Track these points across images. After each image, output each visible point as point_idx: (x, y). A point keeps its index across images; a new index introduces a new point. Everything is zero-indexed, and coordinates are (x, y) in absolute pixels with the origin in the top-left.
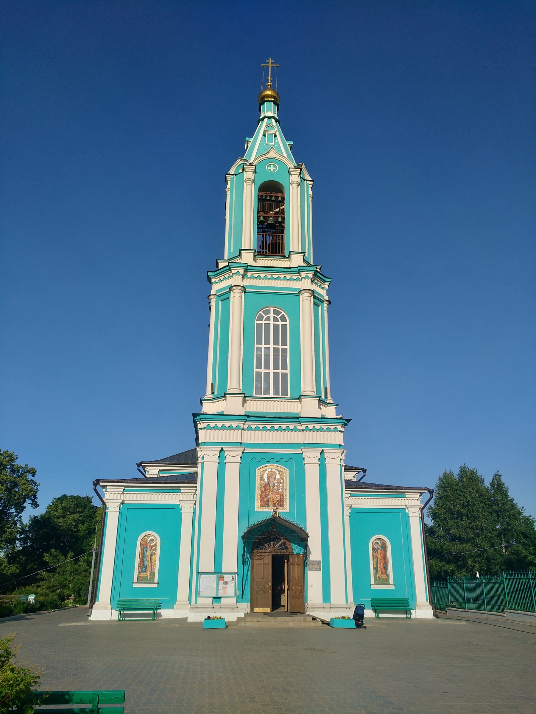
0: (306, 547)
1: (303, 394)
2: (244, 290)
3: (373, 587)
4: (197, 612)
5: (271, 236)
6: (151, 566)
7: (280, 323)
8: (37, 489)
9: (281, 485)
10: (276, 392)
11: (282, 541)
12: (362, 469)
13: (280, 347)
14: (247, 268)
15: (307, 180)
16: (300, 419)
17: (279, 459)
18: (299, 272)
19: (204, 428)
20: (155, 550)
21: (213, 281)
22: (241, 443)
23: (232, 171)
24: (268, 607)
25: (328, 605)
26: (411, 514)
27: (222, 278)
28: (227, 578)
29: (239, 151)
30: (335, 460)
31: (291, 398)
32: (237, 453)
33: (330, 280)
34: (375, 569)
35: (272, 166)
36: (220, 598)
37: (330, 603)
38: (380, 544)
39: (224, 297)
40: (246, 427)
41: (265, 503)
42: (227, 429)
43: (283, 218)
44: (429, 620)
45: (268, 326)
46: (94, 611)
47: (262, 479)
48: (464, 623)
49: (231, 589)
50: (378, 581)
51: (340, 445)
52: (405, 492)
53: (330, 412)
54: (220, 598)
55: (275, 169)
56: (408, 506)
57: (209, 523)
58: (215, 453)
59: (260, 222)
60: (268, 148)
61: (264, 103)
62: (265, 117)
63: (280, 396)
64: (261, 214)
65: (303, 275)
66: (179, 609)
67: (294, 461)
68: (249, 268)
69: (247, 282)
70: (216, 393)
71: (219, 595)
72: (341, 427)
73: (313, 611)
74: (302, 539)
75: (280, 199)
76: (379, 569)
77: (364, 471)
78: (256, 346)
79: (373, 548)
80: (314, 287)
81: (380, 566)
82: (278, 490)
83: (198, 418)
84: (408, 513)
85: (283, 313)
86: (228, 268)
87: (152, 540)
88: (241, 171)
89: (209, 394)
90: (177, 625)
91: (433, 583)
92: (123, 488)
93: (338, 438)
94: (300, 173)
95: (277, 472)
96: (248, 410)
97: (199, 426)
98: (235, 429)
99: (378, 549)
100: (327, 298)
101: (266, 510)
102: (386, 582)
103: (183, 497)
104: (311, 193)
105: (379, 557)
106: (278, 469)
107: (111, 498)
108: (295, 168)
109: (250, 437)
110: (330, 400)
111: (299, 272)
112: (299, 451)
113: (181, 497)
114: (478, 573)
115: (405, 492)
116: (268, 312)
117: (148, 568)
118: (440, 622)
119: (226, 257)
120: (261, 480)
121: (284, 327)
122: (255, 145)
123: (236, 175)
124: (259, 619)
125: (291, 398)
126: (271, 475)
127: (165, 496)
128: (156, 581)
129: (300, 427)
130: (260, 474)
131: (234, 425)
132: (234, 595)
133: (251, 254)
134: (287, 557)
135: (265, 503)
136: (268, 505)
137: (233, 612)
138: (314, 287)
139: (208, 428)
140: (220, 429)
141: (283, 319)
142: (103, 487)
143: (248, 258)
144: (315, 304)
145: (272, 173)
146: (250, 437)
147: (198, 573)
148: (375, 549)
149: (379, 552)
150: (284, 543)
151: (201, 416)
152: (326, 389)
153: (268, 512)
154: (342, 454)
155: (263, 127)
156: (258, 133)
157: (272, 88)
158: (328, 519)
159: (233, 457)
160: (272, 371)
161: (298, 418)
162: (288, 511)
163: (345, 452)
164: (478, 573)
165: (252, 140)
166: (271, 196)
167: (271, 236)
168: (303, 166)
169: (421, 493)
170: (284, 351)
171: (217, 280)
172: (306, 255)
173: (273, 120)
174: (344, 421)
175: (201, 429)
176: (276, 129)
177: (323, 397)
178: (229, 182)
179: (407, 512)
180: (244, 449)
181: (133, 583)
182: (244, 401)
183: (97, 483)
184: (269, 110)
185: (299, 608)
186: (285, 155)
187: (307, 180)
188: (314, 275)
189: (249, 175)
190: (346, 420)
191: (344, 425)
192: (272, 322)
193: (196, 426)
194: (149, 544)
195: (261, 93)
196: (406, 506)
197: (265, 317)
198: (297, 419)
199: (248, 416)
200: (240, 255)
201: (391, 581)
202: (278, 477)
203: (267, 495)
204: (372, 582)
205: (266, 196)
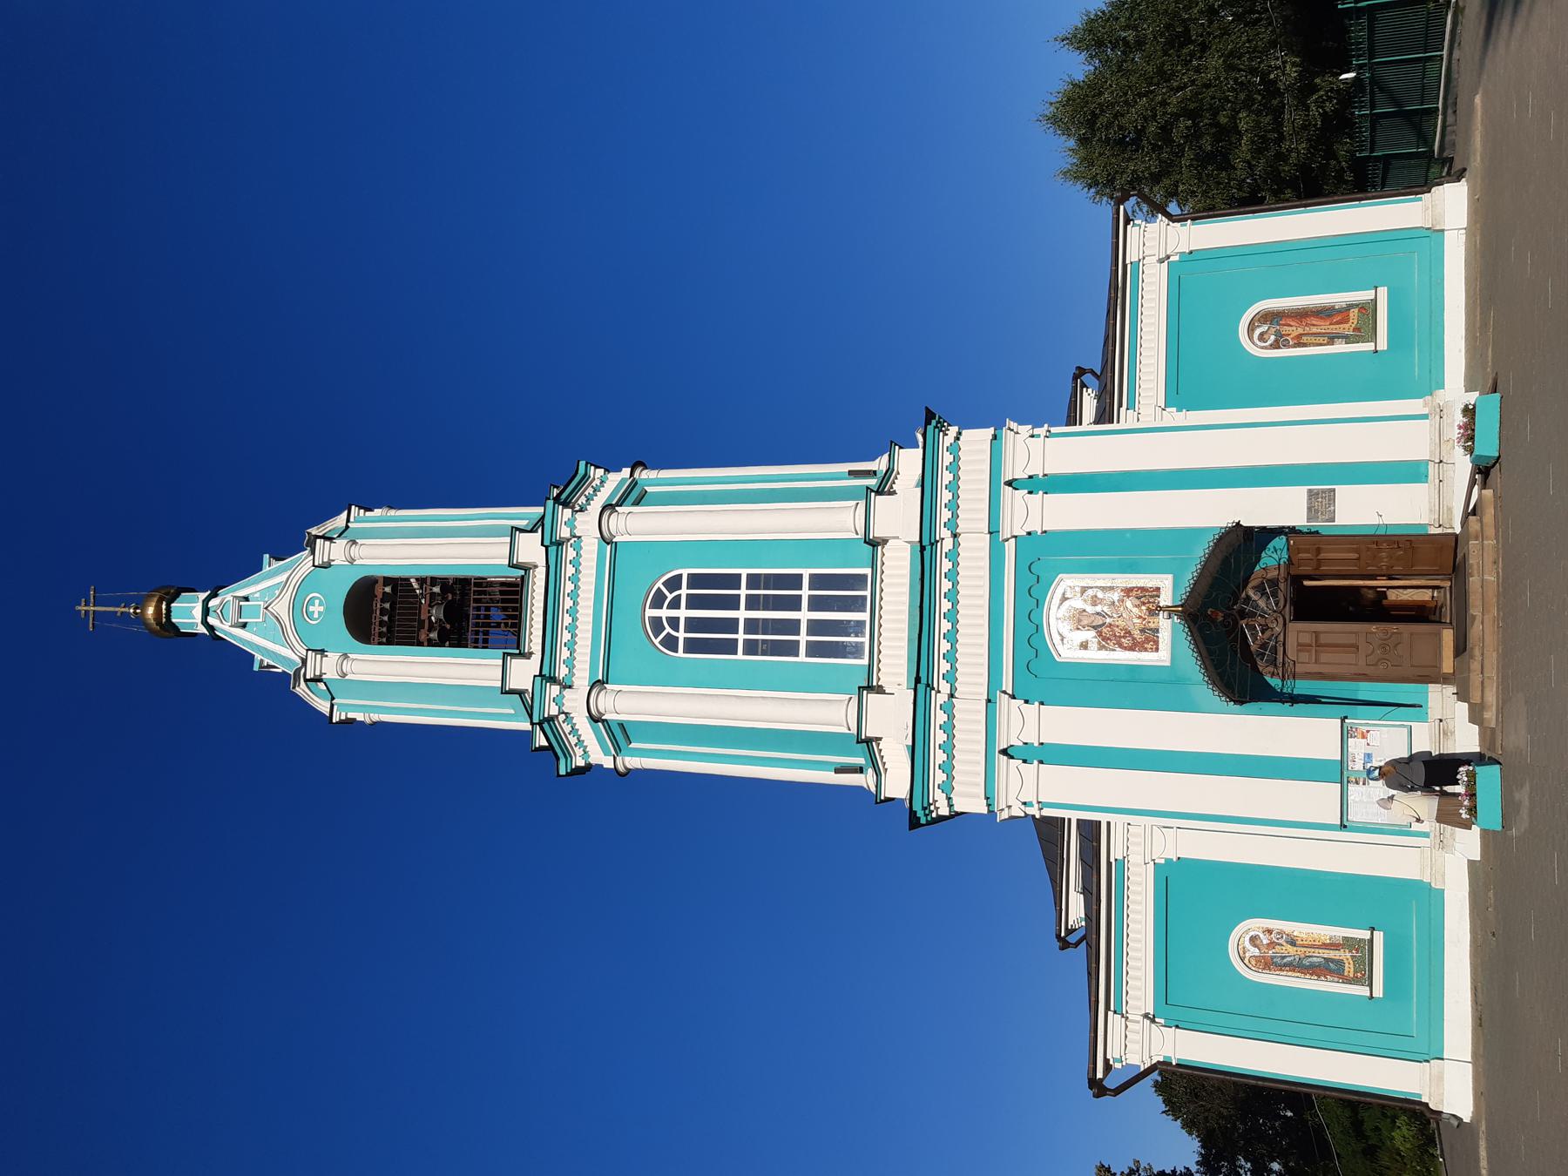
0: (1268, 534)
1: (861, 535)
2: (598, 684)
3: (1382, 344)
5: (472, 612)
6: (1325, 946)
7: (684, 591)
10: (856, 604)
11: (1251, 593)
12: (1075, 378)
14: (547, 677)
16: (926, 542)
18: (560, 543)
19: (949, 799)
21: (581, 763)
22: (989, 701)
23: (323, 706)
24: (1439, 636)
25: (1432, 470)
27: (573, 740)
29: (278, 685)
30: (1032, 449)
31: (873, 566)
32: (1015, 713)
33: (582, 464)
34: (1332, 339)
35: (311, 609)
39: (619, 734)
40: (945, 688)
41: (1149, 640)
43: (434, 581)
46: (1447, 1109)
50: (1366, 330)
51: (995, 437)
52: (1125, 266)
56: (1163, 256)
60: (275, 614)
61: (174, 627)
62: (205, 622)
63: (867, 593)
64: (423, 637)
65: (565, 532)
66: (1443, 876)
67: (1039, 560)
69: (582, 681)
73: (1450, 509)
74: (1241, 545)
75: (388, 589)
77: (1081, 372)
79: (1276, 346)
81: (1324, 327)
83: (920, 814)
86: (546, 725)
87: (1253, 940)
88: (322, 686)
89: (866, 780)
90: (1491, 894)
93: (976, 440)
94: (331, 539)
95: (1067, 603)
96: (903, 679)
97: (944, 811)
98: (951, 717)
99: (1279, 335)
101: (1165, 637)
102: (1368, 310)
103: (1137, 852)
104: (377, 512)
105: (1300, 331)
107: (1138, 1047)
108: (313, 553)
111: (560, 543)
113: (1135, 859)
115: (1125, 266)
116: (657, 624)
117: (1332, 954)
118: (1476, 162)
119: (526, 726)
121: (695, 581)
122: (270, 647)
124: (1475, 665)
125: (873, 566)
126: (1079, 619)
127: (1135, 902)
128: (1366, 935)
129: (948, 544)
131: (941, 717)
132: (1405, 731)
133: (516, 665)
135: (1149, 640)
137: (1453, 733)
140: (951, 757)
142: (1108, 1067)
143: (523, 673)
144: (637, 503)
145: (327, 608)
147: (1343, 826)
148: (1276, 341)
149: (1285, 330)
150: (1260, 589)
151: (917, 807)
152: (854, 474)
153: (1168, 628)
155: (225, 628)
156: (241, 640)
157: (141, 604)
159: (1024, 722)
161: (923, 549)
163: (1014, 425)
165: (258, 657)
166: (383, 611)
167: (472, 612)
168: (314, 531)
169: (1127, 222)
171: (579, 751)
172: (522, 523)
173: (213, 603)
174: (930, 428)
175: (951, 806)
176: (229, 598)
178: (350, 715)
179: (1176, 258)
181: (1371, 997)
182: (880, 690)
183: (1098, 1088)
184: (188, 612)
185: (1441, 555)
186: (283, 577)
189: (329, 666)
190: (928, 422)
191: (941, 428)
192: (683, 613)
193: (941, 819)
195: (152, 631)
197: (668, 629)
198: (925, 549)
199: (918, 680)
200: (520, 693)
201: (1367, 295)
202: (1078, 603)
204: (1370, 346)
205: (382, 623)
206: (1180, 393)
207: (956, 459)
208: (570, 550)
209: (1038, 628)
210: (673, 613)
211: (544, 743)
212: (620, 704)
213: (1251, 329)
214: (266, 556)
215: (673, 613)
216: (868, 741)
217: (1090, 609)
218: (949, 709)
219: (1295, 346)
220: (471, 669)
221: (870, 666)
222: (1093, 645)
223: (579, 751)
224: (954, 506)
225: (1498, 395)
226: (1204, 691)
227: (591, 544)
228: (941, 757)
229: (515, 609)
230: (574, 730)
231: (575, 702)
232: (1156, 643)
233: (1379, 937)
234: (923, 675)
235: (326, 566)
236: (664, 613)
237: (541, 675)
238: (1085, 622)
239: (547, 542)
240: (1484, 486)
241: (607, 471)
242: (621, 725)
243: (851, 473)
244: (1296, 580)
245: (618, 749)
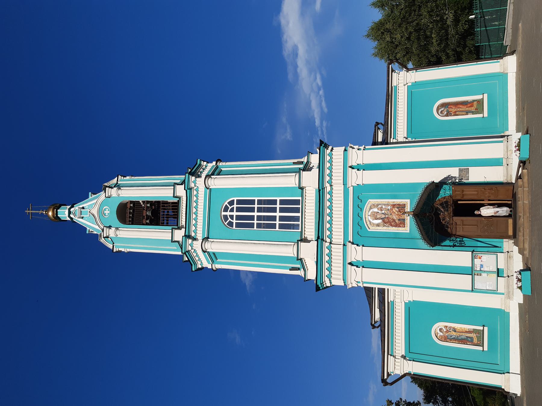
1: (297, 186)
2: (206, 239)
3: (486, 115)
4: (513, 294)
5: (160, 214)
6: (466, 332)
7: (235, 206)
8: (404, 402)
9: (384, 207)
10: (297, 210)
12: (375, 126)
13: (256, 206)
14: (188, 236)
15: (117, 181)
16: (321, 188)
17: (359, 208)
19: (330, 280)
20: (451, 327)
21: (200, 266)
22: (344, 245)
23: (110, 246)
27: (197, 259)
28: (477, 262)
30: (360, 155)
31: (302, 196)
33: (199, 160)
35: (105, 212)
36: (498, 269)
37: (502, 158)
38: (442, 109)
39: (213, 257)
41: (402, 223)
42: (331, 258)
44: (518, 59)
45: (238, 218)
46: (512, 391)
47: (378, 225)
48: (520, 25)
49: (487, 261)
50: (479, 109)
51: (345, 150)
53: (314, 159)
54: (498, 269)
57: (421, 280)
58: (353, 271)
59: (151, 224)
60: (93, 213)
62: (69, 216)
65: (192, 185)
67: (361, 194)
68: (187, 234)
69: (200, 237)
70: (298, 266)
71: (496, 270)
72: (327, 149)
73: (511, 176)
74: (434, 188)
77: (377, 124)
79: (447, 115)
80: (204, 175)
81: (464, 108)
82: (388, 210)
83: (320, 286)
84: (412, 83)
86: (187, 253)
89: (301, 273)
90: (527, 316)
91: (482, 58)
92: (389, 356)
93: (338, 151)
95: (372, 210)
100: (214, 163)
102: (480, 102)
103: (399, 299)
106: (368, 209)
109: (338, 236)
110: (305, 160)
111: (191, 189)
112: (351, 189)
116: (226, 217)
118: (519, 48)
120: (379, 226)
121: (239, 202)
122: (92, 226)
125: (302, 196)
127: (398, 316)
128: (481, 328)
129: (329, 189)
130: (374, 228)
131: (327, 251)
132: (495, 256)
133: (176, 232)
134: (455, 202)
135: (402, 223)
136: (404, 220)
137: (513, 257)
138: (204, 175)
139: (330, 277)
142: (389, 375)
143: (179, 235)
144: (219, 174)
145: (110, 212)
146: (338, 236)
148: (447, 114)
149: (450, 110)
151: (319, 283)
152: (294, 163)
153: (409, 220)
154: (353, 148)
157: (47, 211)
158: (414, 165)
159: (356, 253)
160: (275, 215)
161: (319, 190)
162: (408, 232)
165: (88, 229)
167: (160, 214)
168: (106, 184)
169: (393, 71)
170: (260, 202)
171: (199, 263)
173: (72, 210)
174: (322, 147)
175: (331, 283)
176: (77, 208)
177: (301, 166)
178: (120, 249)
179: (410, 84)
180: (350, 242)
184: (63, 213)
187: (117, 181)
188: (193, 175)
189: (112, 233)
190: (321, 145)
191: (326, 146)
192: (235, 214)
195: (51, 220)
196: (405, 85)
197: (230, 219)
198: (321, 191)
199: (318, 238)
200: (178, 242)
201: (479, 97)
202: (376, 210)
203: (394, 220)
204: (481, 115)
205: (130, 217)
210: (231, 213)
211: (187, 259)
214: (90, 193)
215: (231, 213)
216: (301, 259)
217: (380, 212)
221: (301, 232)
223: (199, 263)
224: (331, 176)
226: (422, 243)
227: (202, 188)
228: (327, 265)
233: (486, 329)
234: (320, 235)
235: (109, 197)
236: (228, 213)
237: (185, 236)
238: (378, 217)
239: (186, 189)
241: (208, 162)
242: (214, 253)
245: (213, 262)
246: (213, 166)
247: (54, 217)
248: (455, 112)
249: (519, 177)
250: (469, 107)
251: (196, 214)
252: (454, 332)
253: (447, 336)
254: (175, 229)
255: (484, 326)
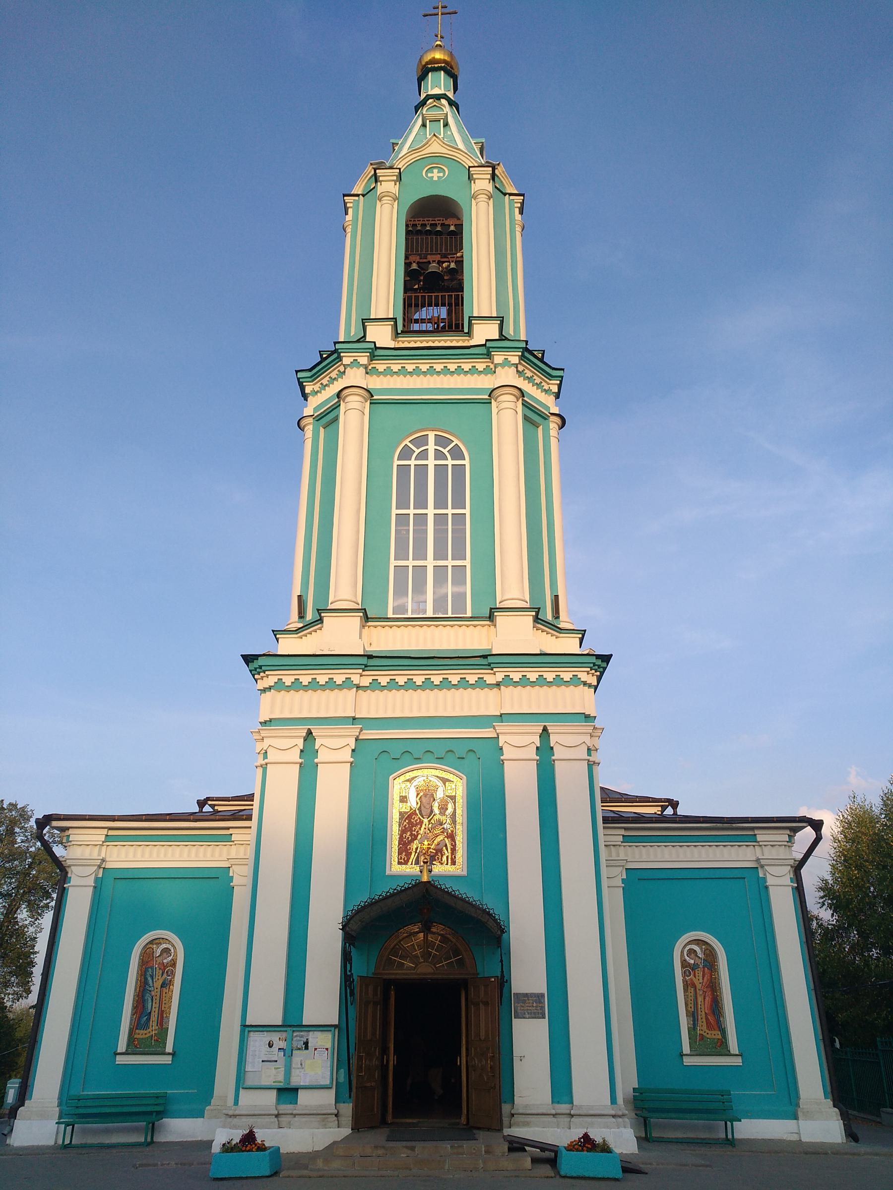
7: (450, 462)
14: (375, 353)
15: (510, 194)
16: (491, 659)
19: (270, 688)
20: (173, 974)
21: (308, 390)
22: (354, 718)
25: (563, 1108)
26: (770, 881)
27: (325, 382)
31: (472, 618)
34: (693, 1015)
35: (435, 171)
39: (329, 418)
42: (323, 687)
46: (19, 1124)
47: (403, 799)
49: (317, 1066)
50: (701, 1046)
52: (753, 829)
54: (295, 1090)
55: (441, 175)
58: (293, 742)
62: (429, 97)
65: (498, 358)
69: (374, 383)
70: (310, 616)
71: (295, 1081)
73: (526, 1124)
76: (701, 1015)
78: (395, 511)
81: (704, 1005)
84: (765, 879)
85: (456, 442)
86: (335, 356)
87: (167, 951)
92: (105, 831)
95: (440, 783)
98: (340, 687)
99: (694, 967)
100: (556, 410)
105: (699, 986)
109: (375, 704)
111: (489, 355)
112: (488, 733)
114: (837, 1040)
115: (753, 829)
116: (422, 441)
117: (154, 1017)
121: (459, 471)
123: (363, 195)
125: (472, 618)
126: (427, 795)
128: (169, 1048)
129: (490, 679)
131: (339, 679)
132: (327, 1082)
135: (403, 862)
137: (325, 1127)
141: (457, 453)
142: (63, 829)
143: (381, 335)
144: (526, 418)
145: (435, 181)
146: (375, 704)
147: (244, 1026)
159: (335, 751)
164: (837, 1040)
166: (434, 233)
170: (459, 519)
171: (317, 387)
174: (593, 659)
177: (549, 617)
181: (116, 1054)
186: (461, 146)
189: (388, 186)
192: (431, 462)
194: (159, 960)
197: (417, 451)
198: (485, 660)
199: (370, 657)
200: (365, 336)
201: (734, 1047)
202: (440, 794)
204: (686, 1049)
205: (424, 225)
206: (638, 882)
207: (567, 683)
208: (484, 366)
209: (418, 760)
210: (431, 454)
212: (354, 419)
213: (698, 942)
215: (431, 454)
216: (321, 620)
218: (347, 684)
219: (685, 981)
220: (385, 292)
221: (388, 619)
222: (405, 808)
223: (317, 387)
224: (524, 682)
225: (619, 1174)
226: (362, 898)
227: (487, 382)
228: (305, 680)
229: (450, 327)
230: (333, 380)
231: (355, 377)
232: (406, 863)
233: (167, 1060)
235: (470, 177)
236: (431, 447)
237: (377, 348)
239: (488, 344)
240: (535, 1161)
242: (336, 419)
243: (557, 597)
244: (464, 984)
245: (319, 418)
246: (548, 408)
247: (427, 63)
248: (694, 985)
249: (517, 1146)
250: (707, 1019)
251: (431, 371)
252: (160, 982)
253: (152, 968)
254: (395, 326)
255: (173, 1054)
